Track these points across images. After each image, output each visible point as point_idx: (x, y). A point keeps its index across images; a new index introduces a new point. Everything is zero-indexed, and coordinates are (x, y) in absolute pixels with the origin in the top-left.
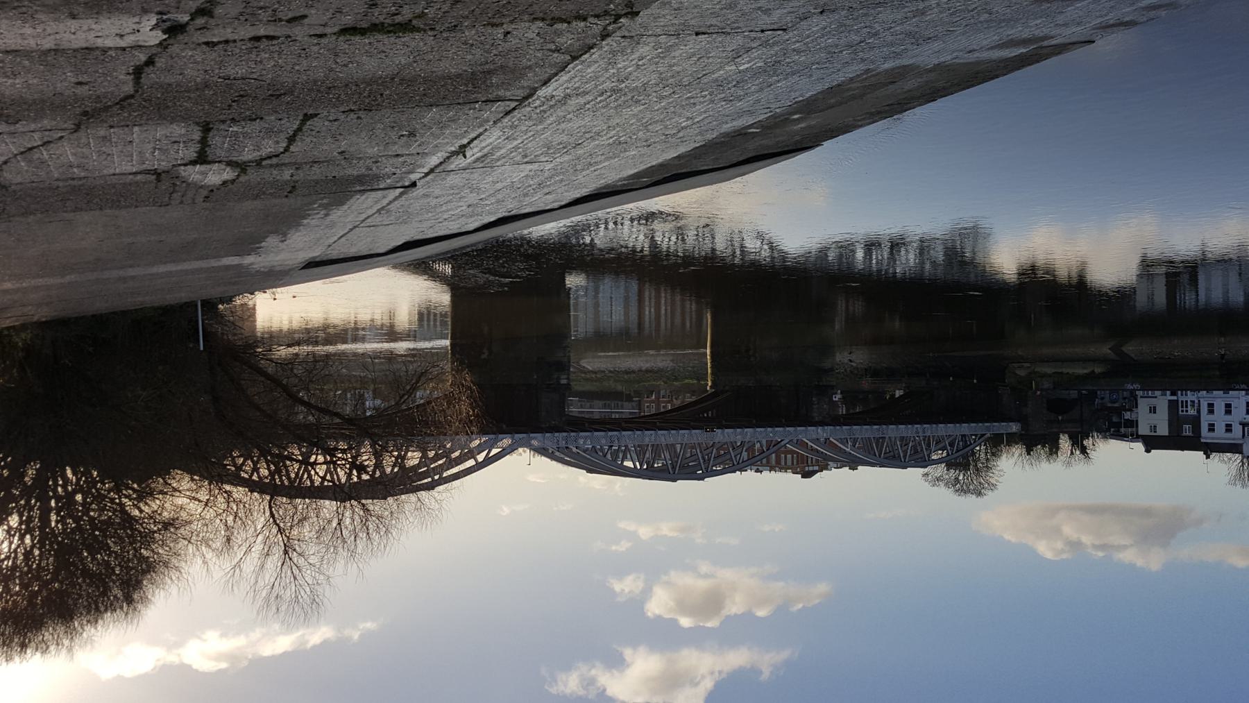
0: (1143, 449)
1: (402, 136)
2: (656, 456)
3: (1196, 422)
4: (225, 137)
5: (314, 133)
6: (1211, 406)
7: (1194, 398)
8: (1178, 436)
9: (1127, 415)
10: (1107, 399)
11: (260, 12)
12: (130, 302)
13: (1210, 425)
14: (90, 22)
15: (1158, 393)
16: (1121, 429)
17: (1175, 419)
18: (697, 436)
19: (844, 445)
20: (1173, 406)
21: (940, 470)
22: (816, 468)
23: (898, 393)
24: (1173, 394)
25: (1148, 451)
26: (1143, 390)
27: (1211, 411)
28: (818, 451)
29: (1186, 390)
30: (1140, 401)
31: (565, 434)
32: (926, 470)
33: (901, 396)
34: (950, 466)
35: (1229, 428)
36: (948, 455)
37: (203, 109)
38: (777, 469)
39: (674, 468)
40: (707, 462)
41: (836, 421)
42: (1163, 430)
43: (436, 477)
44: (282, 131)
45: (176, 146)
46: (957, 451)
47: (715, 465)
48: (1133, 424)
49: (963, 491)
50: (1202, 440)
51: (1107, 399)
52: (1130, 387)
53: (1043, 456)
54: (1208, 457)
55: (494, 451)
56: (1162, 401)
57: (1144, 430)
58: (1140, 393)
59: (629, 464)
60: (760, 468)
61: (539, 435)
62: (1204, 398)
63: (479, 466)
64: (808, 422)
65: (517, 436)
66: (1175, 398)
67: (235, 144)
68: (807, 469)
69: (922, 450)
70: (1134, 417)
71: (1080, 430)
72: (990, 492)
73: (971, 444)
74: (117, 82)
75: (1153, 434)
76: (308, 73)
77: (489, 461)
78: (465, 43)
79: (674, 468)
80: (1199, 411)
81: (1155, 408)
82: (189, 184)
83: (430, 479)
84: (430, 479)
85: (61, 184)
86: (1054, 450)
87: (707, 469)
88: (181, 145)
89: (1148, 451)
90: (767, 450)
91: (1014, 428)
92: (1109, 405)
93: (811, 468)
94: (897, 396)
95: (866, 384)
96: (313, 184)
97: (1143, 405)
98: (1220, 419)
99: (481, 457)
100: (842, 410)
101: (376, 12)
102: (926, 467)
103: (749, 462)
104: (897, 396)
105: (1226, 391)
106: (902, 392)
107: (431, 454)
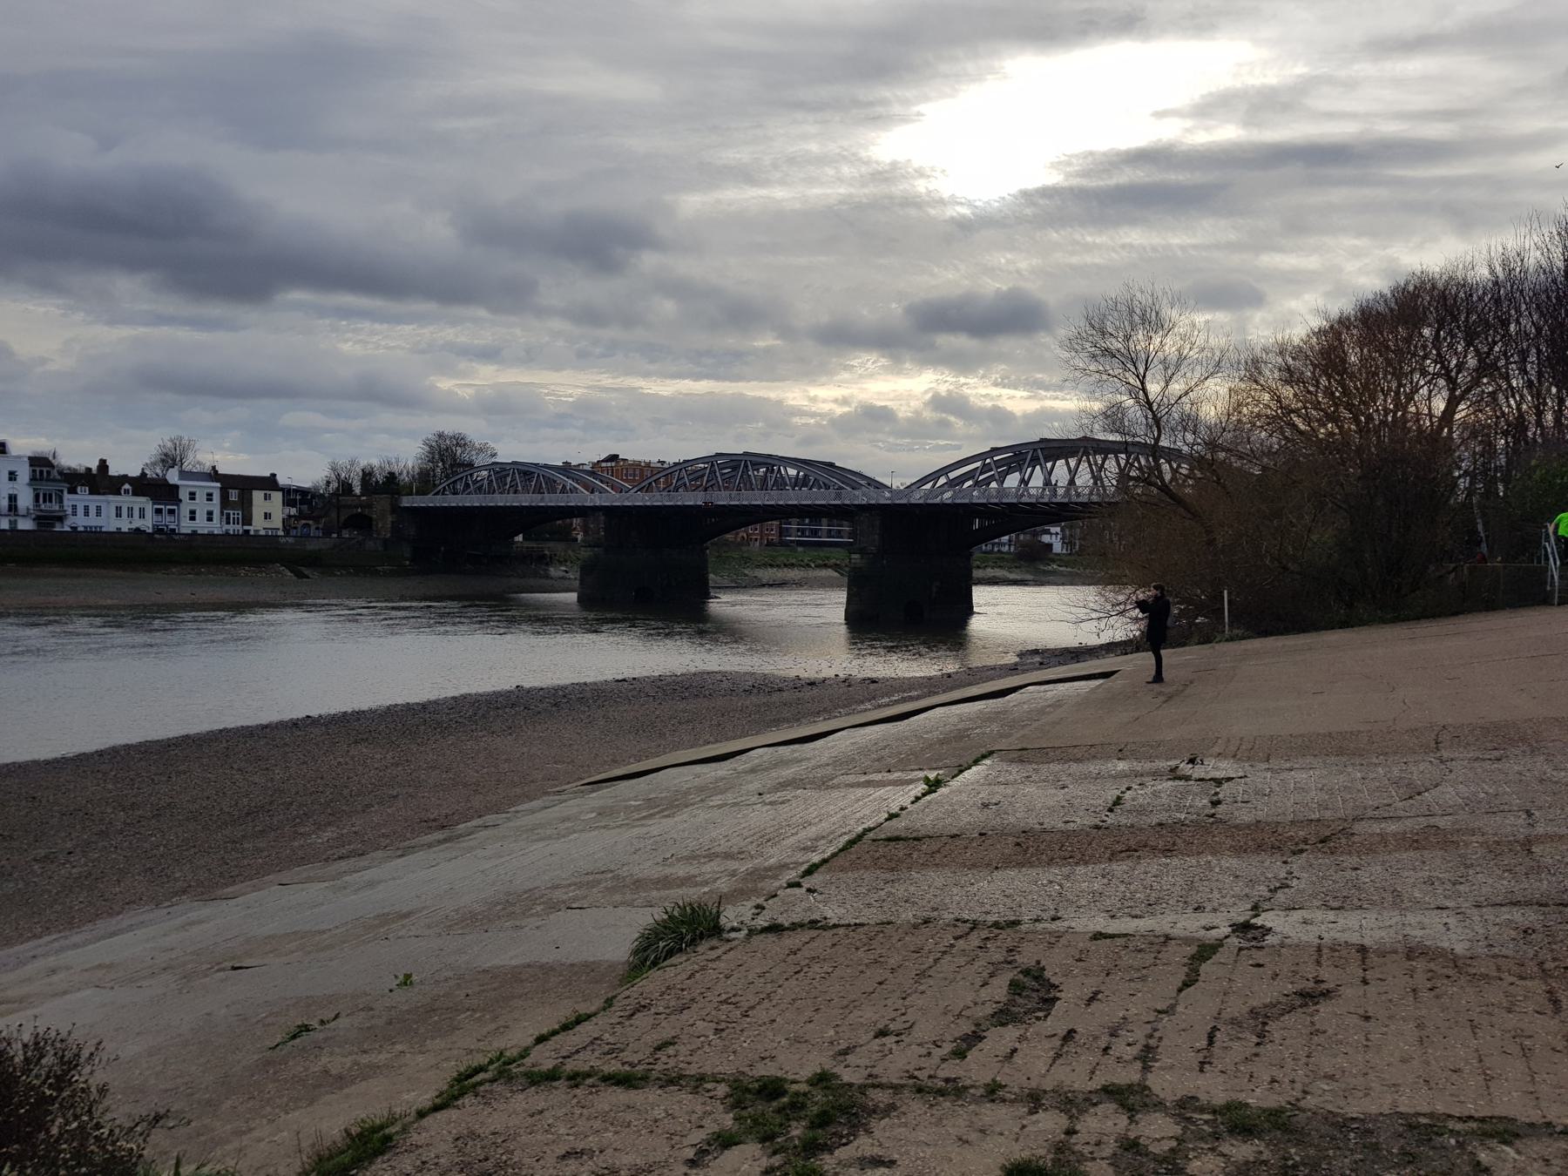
0: (278, 478)
1: (996, 804)
2: (765, 479)
3: (225, 502)
4: (1191, 806)
5: (1092, 809)
6: (210, 519)
7: (227, 527)
8: (243, 490)
9: (293, 511)
10: (313, 528)
11: (1143, 946)
12: (1310, 634)
13: (211, 500)
14: (776, 672)
15: (262, 533)
16: (294, 496)
17: (246, 505)
18: (722, 498)
19: (575, 487)
20: (247, 520)
21: (479, 460)
22: (604, 464)
23: (520, 538)
24: (248, 531)
25: (274, 475)
26: (277, 536)
27: (210, 514)
28: (602, 482)
29: (234, 535)
30: (280, 525)
31: (856, 502)
32: (493, 460)
33: (517, 535)
34: (471, 465)
35: (192, 496)
36: (471, 475)
37: (1214, 836)
38: (643, 464)
39: (746, 466)
40: (713, 472)
41: (582, 511)
42: (258, 496)
43: (988, 461)
44: (1128, 811)
45: (1246, 798)
46: (462, 478)
47: (705, 468)
48: (288, 502)
49: (460, 441)
50: (219, 485)
51: (313, 528)
52: (290, 540)
53: (377, 472)
54: (214, 468)
55: (928, 486)
56: (258, 525)
57: (277, 497)
58: (281, 533)
59: (792, 472)
60: (659, 465)
61: (882, 501)
62: (217, 527)
63: (945, 471)
64: (609, 511)
65: (904, 501)
66: (246, 528)
67: (1180, 799)
68: (613, 464)
69: (497, 480)
70: (287, 510)
71: (341, 498)
72: (430, 436)
73: (448, 485)
74: (1310, 869)
75: (268, 492)
76: (1093, 875)
77: (935, 476)
78: (914, 903)
79: (746, 466)
80: (222, 513)
81: (266, 518)
82: (1234, 756)
83: (995, 458)
84: (995, 458)
85: (1375, 760)
86: (367, 475)
87: (713, 465)
88: (1239, 799)
89: (274, 475)
90: (650, 483)
91: (406, 502)
92: (311, 522)
93: (609, 464)
94: (521, 536)
95: (549, 547)
96: (1099, 755)
97: (277, 522)
98: (201, 506)
99: (942, 480)
100: (576, 522)
101: (1009, 943)
102: (494, 463)
103: (670, 471)
104: (521, 536)
105: (194, 533)
106: (516, 539)
107: (994, 485)
